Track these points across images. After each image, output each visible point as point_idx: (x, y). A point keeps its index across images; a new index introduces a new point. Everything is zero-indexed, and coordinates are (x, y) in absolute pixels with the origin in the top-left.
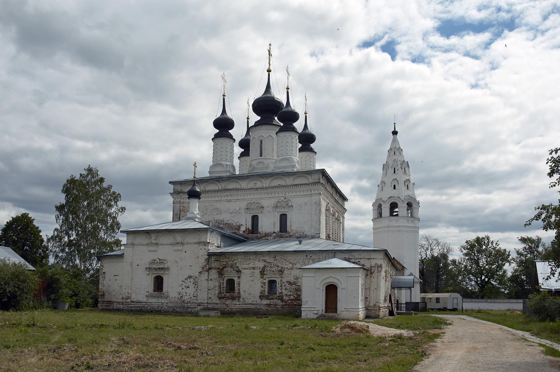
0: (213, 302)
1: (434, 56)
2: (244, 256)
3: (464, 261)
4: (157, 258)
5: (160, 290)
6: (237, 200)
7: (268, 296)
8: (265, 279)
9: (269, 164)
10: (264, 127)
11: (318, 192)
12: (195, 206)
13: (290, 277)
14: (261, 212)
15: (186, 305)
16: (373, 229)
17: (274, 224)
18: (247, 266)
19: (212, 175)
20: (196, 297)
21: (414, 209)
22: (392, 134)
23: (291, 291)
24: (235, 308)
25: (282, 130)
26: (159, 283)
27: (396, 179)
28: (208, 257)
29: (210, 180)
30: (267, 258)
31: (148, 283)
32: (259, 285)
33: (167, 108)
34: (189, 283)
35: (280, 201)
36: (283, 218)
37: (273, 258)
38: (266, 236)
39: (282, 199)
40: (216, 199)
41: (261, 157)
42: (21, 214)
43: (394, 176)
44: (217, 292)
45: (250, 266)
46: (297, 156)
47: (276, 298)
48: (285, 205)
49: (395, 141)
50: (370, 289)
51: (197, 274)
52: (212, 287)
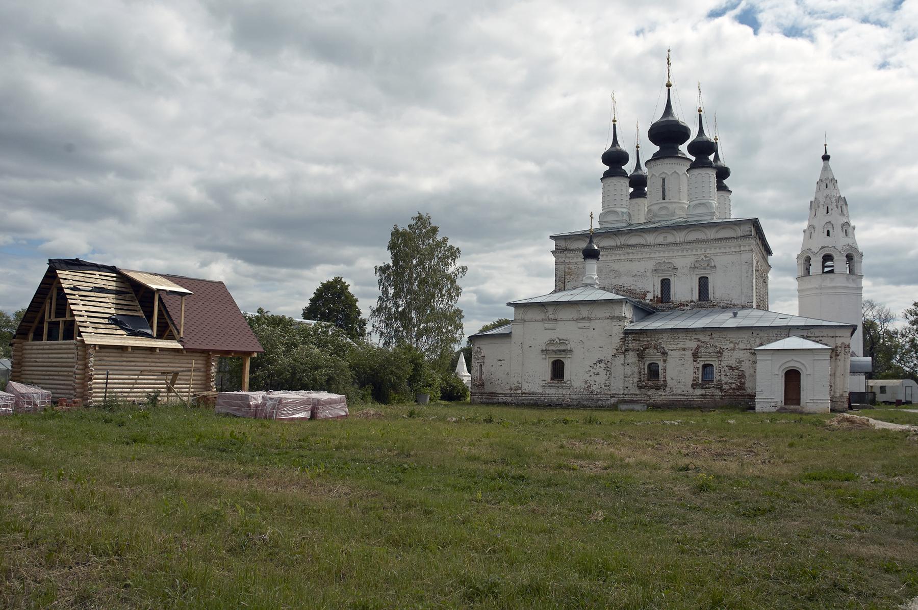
0: (631, 392)
1: (816, 26)
2: (671, 333)
3: (910, 332)
4: (555, 337)
5: (560, 378)
6: (641, 260)
7: (704, 385)
8: (699, 363)
9: (675, 209)
10: (667, 161)
11: (750, 248)
12: (592, 268)
13: (731, 360)
14: (674, 275)
15: (595, 397)
16: (799, 291)
17: (692, 290)
18: (675, 347)
19: (603, 226)
20: (608, 386)
21: (856, 264)
22: (822, 160)
23: (732, 378)
24: (660, 400)
25: (694, 166)
26: (558, 370)
27: (830, 222)
28: (624, 335)
29: (605, 234)
30: (701, 337)
31: (545, 370)
32: (691, 370)
33: (428, 115)
34: (600, 368)
35: (699, 259)
36: (703, 283)
37: (709, 336)
38: (681, 306)
39: (701, 258)
40: (613, 258)
41: (664, 201)
42: (334, 278)
43: (828, 219)
44: (636, 380)
45: (679, 346)
46: (716, 199)
47: (713, 387)
48: (706, 265)
49: (826, 169)
50: (835, 376)
51: (609, 358)
52: (629, 373)
